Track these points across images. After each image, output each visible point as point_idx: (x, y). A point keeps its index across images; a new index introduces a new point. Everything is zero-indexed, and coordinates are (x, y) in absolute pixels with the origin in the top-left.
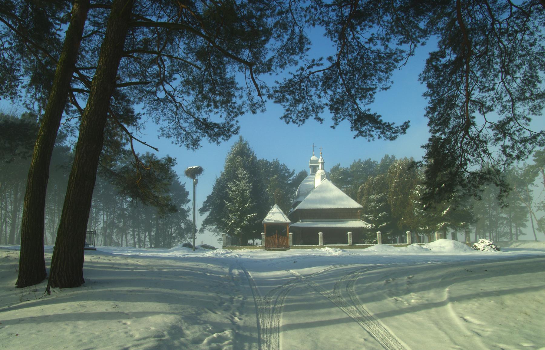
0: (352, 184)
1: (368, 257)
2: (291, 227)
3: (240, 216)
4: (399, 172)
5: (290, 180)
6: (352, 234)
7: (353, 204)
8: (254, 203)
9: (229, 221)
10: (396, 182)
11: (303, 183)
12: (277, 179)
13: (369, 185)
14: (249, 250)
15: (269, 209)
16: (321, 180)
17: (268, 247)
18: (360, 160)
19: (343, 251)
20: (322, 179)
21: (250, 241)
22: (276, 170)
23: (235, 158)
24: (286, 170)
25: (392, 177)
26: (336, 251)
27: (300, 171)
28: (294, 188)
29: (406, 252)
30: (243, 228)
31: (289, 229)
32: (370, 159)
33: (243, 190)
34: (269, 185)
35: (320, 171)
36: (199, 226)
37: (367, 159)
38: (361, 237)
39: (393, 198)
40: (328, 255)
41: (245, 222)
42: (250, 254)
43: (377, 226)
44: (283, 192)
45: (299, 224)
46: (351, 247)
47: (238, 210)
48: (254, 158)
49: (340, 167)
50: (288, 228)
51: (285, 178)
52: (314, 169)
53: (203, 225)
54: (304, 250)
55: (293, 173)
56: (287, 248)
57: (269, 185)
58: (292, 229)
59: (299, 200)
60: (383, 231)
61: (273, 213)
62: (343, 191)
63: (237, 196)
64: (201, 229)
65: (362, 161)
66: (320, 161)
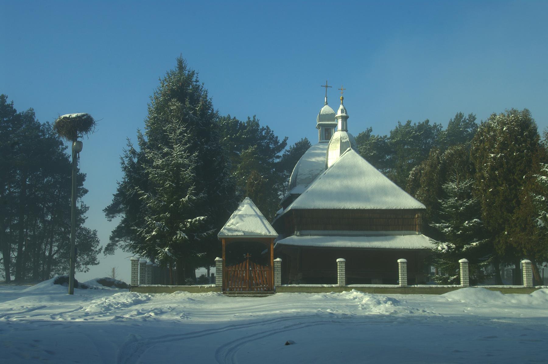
0: (392, 167)
1: (452, 318)
2: (279, 245)
3: (169, 222)
4: (500, 139)
5: (278, 157)
6: (407, 263)
7: (409, 202)
8: (202, 195)
9: (147, 232)
10: (494, 158)
11: (304, 158)
12: (253, 153)
13: (431, 166)
14: (188, 295)
15: (235, 207)
16: (341, 153)
17: (230, 287)
18: (409, 122)
19: (395, 302)
20: (342, 150)
21: (200, 272)
22: (253, 137)
23: (166, 101)
24: (271, 139)
25: (484, 149)
26: (379, 303)
27: (298, 140)
28: (285, 172)
29: (530, 306)
30: (175, 247)
31: (275, 250)
32: (428, 121)
33: (179, 166)
34: (239, 166)
35: (338, 135)
36: (104, 239)
37: (422, 121)
38: (422, 270)
39: (485, 191)
40: (360, 312)
41: (180, 235)
42: (187, 305)
43: (459, 248)
44: (265, 178)
45: (295, 239)
46: (404, 291)
47: (165, 209)
48: (207, 106)
49: (371, 134)
50: (273, 247)
51: (270, 153)
52: (327, 132)
53: (112, 238)
54: (304, 295)
55: (284, 144)
56: (270, 290)
57: (239, 166)
58: (281, 251)
59: (294, 192)
60: (474, 257)
61: (241, 217)
62: (384, 173)
63: (164, 177)
64: (109, 245)
65: (412, 124)
66: (339, 114)
